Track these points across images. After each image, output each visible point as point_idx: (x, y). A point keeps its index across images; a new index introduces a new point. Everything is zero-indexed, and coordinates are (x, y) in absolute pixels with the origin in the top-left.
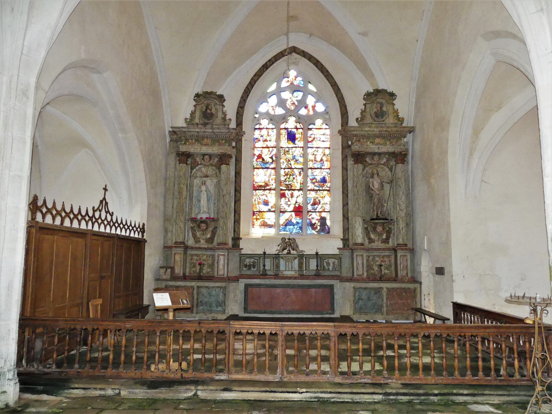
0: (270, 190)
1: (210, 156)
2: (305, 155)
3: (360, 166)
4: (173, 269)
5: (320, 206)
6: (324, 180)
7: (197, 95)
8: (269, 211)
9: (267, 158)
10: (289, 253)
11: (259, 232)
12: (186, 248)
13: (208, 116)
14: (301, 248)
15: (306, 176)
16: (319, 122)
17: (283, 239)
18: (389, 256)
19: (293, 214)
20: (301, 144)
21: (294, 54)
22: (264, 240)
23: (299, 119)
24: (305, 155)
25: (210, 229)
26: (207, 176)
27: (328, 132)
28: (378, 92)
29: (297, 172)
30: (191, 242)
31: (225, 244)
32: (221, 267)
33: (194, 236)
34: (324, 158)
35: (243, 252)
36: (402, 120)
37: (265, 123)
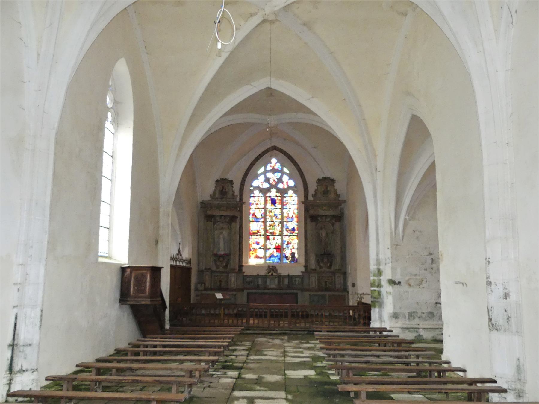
0: (260, 235)
1: (225, 216)
2: (282, 214)
3: (314, 223)
4: (205, 284)
5: (292, 245)
6: (294, 229)
7: (217, 181)
8: (260, 248)
9: (259, 216)
10: (272, 275)
11: (255, 259)
12: (212, 272)
13: (223, 193)
14: (279, 271)
15: (282, 227)
16: (290, 192)
17: (269, 267)
18: (331, 277)
19: (275, 250)
20: (280, 206)
21: (275, 151)
22: (257, 267)
23: (279, 190)
24: (282, 214)
25: (226, 260)
26: (222, 228)
27: (296, 199)
28: (324, 179)
29: (277, 224)
30: (214, 268)
31: (235, 269)
32: (232, 283)
33: (216, 264)
34: (294, 216)
35: (245, 274)
36: (338, 196)
37: (256, 193)
